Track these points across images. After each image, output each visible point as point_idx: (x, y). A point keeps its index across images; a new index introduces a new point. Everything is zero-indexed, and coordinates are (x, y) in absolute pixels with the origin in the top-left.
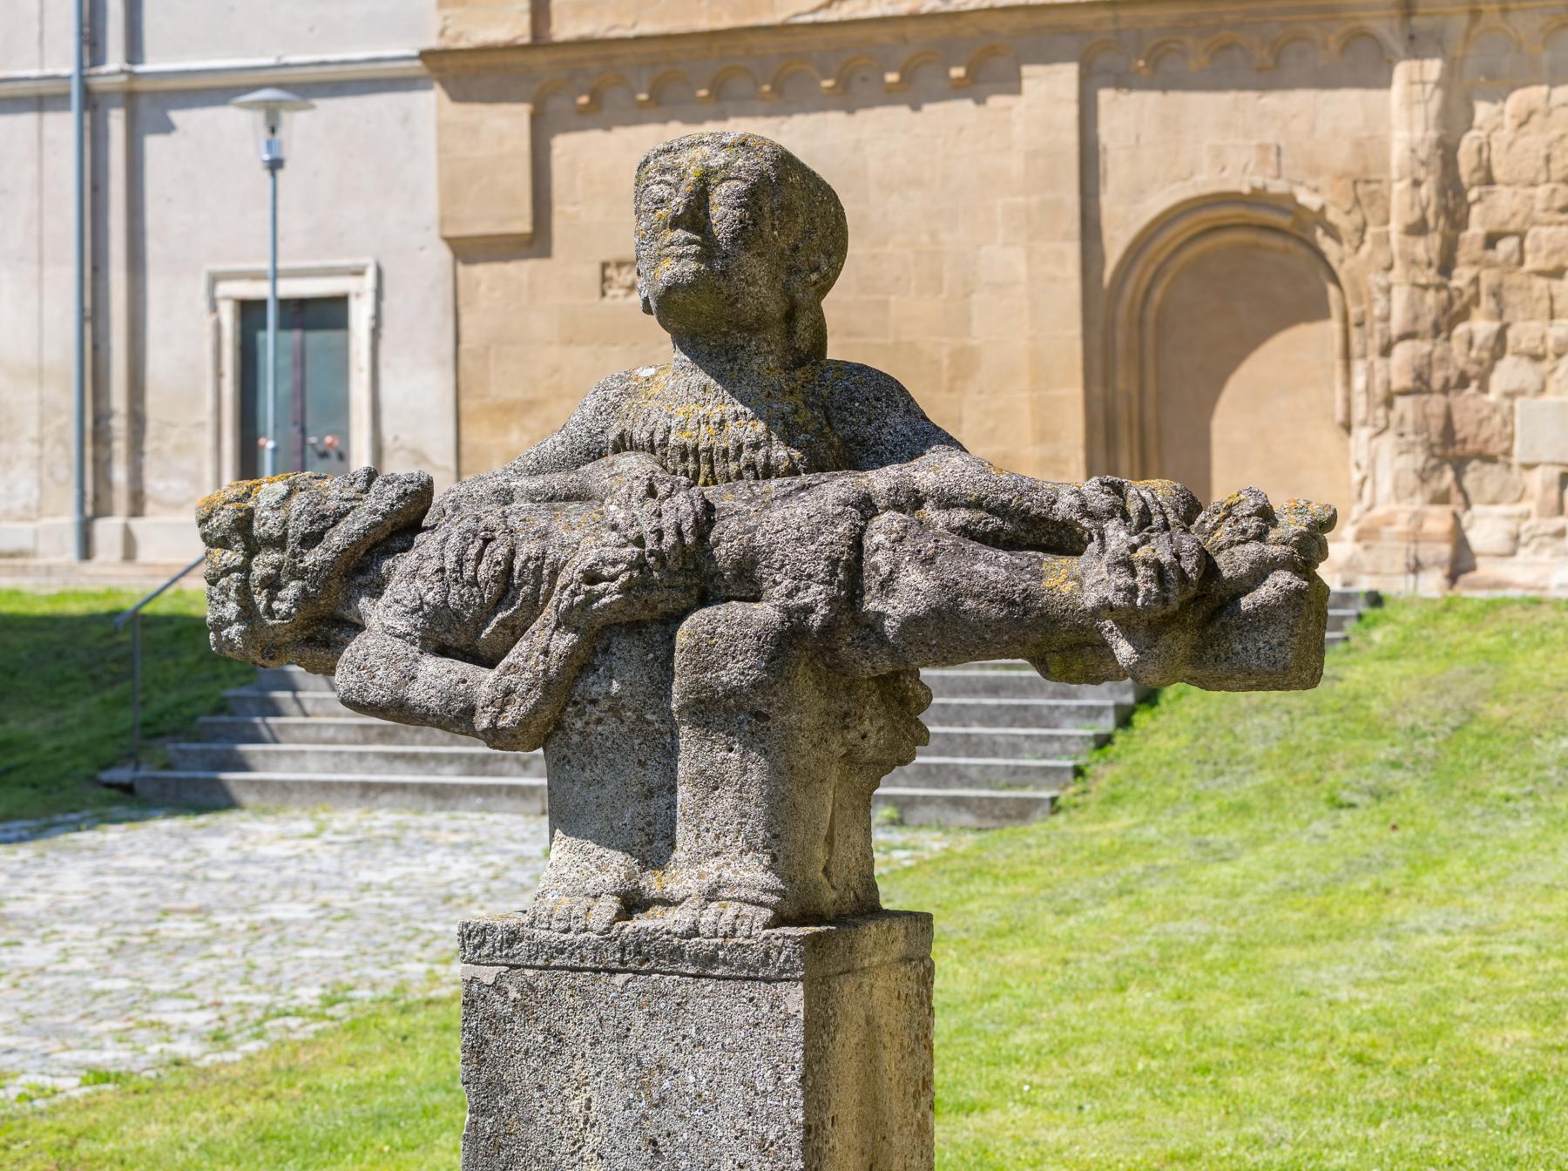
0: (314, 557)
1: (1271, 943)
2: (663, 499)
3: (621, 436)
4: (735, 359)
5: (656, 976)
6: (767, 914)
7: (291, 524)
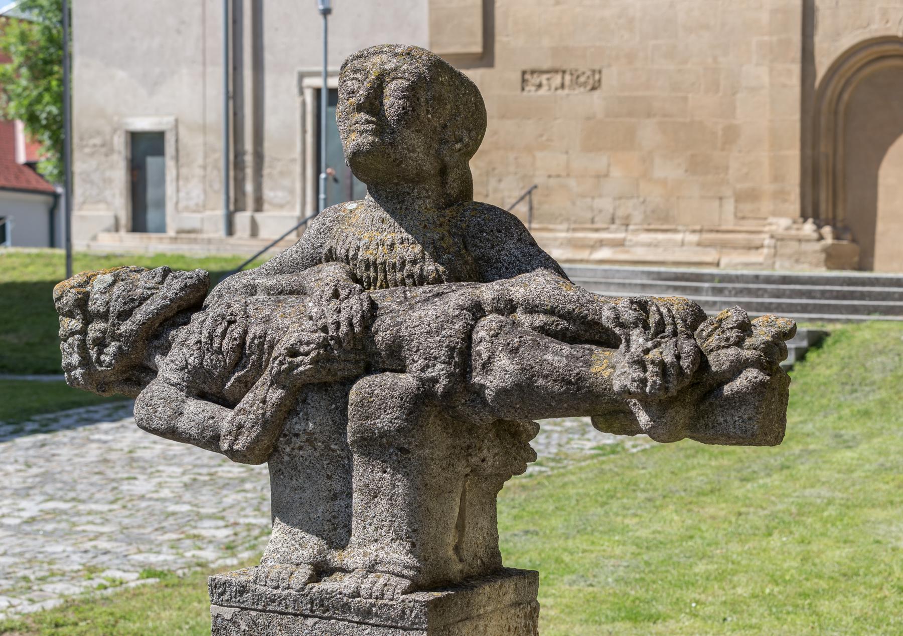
0: (125, 327)
1: (866, 505)
2: (342, 301)
3: (330, 250)
4: (403, 201)
5: (333, 621)
6: (407, 583)
7: (112, 304)
